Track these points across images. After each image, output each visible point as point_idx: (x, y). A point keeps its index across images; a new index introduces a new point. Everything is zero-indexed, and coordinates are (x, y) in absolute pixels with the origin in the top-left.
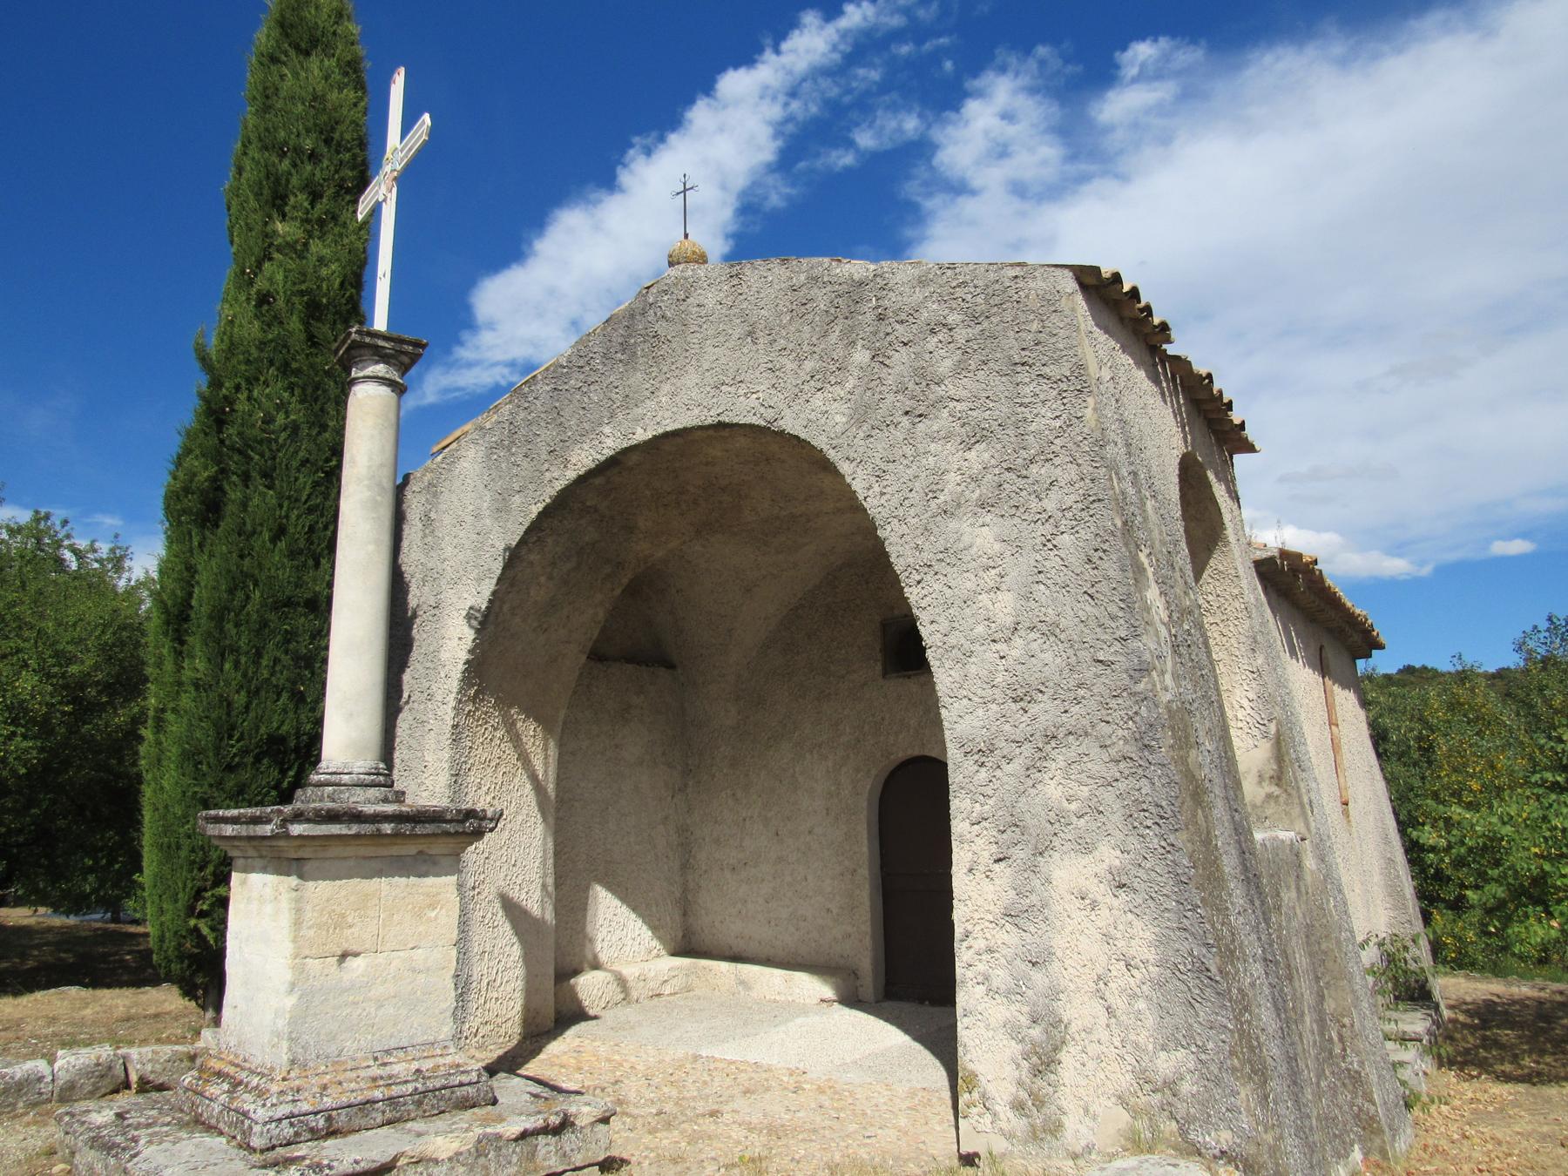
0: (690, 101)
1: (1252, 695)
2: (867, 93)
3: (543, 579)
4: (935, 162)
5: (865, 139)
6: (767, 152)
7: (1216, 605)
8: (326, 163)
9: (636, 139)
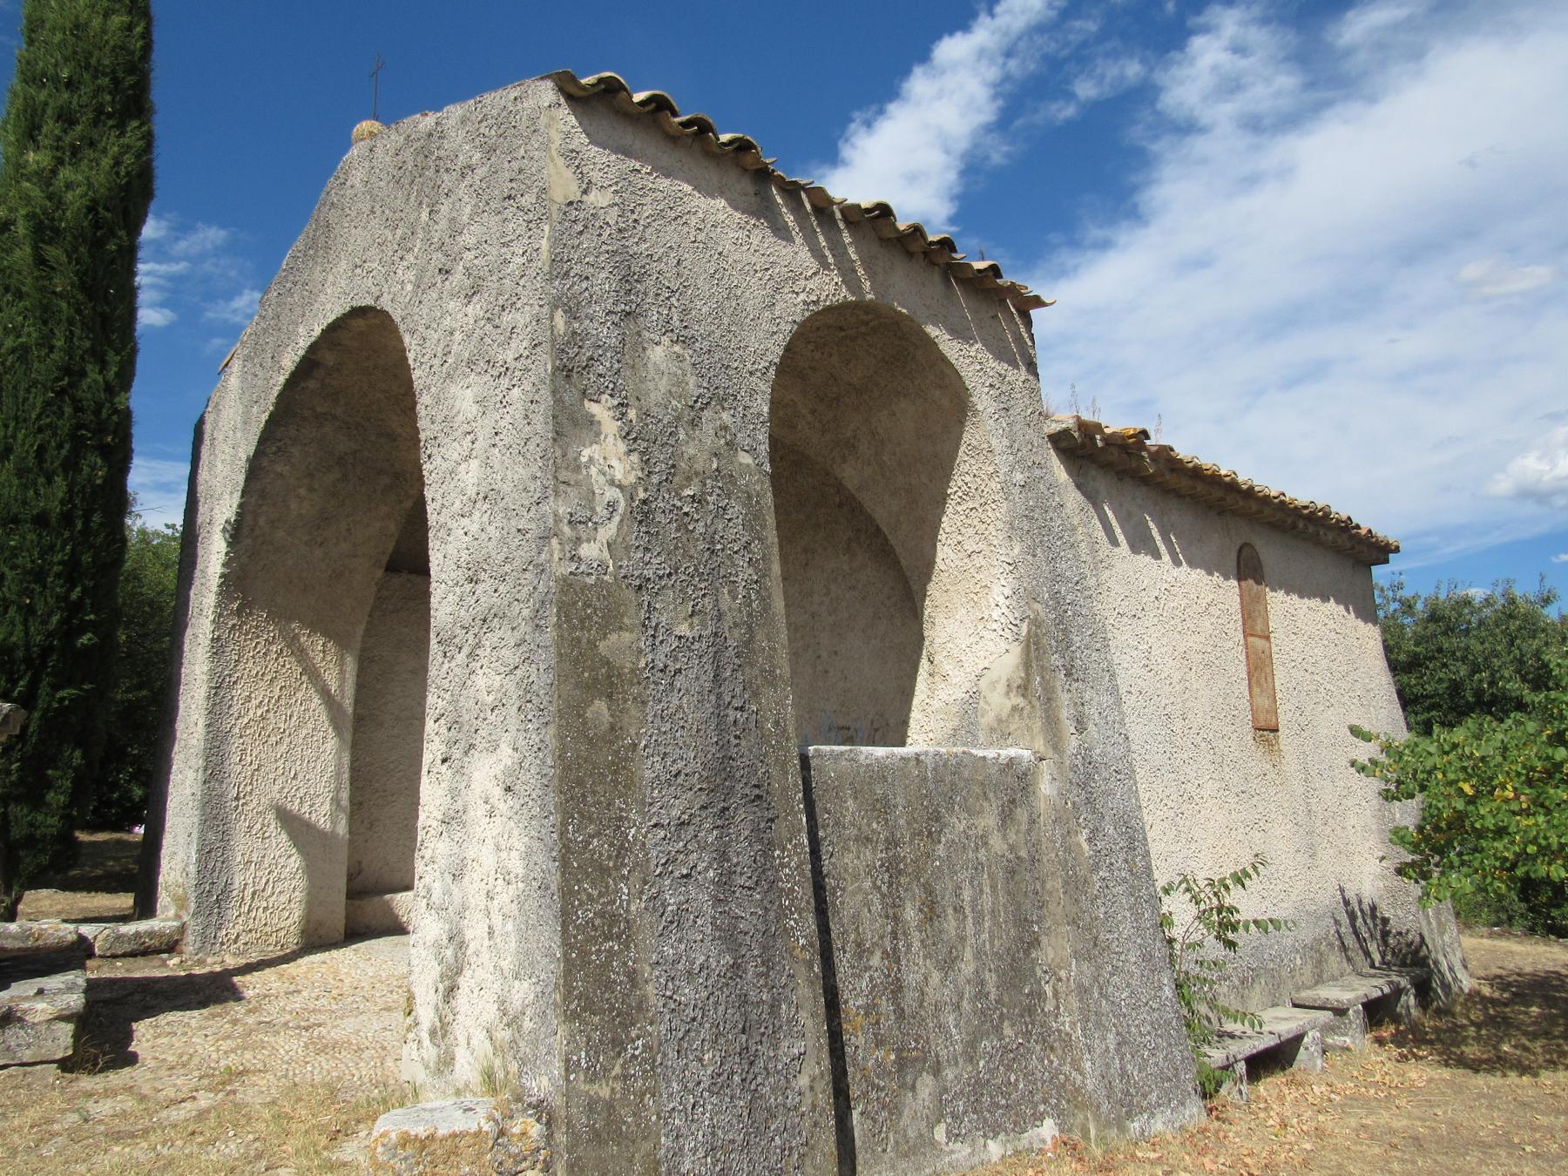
0: (906, 73)
1: (1008, 592)
2: (1084, 44)
3: (302, 491)
4: (1159, 106)
5: (1086, 89)
6: (987, 113)
7: (974, 486)
8: (83, 90)
9: (856, 114)
